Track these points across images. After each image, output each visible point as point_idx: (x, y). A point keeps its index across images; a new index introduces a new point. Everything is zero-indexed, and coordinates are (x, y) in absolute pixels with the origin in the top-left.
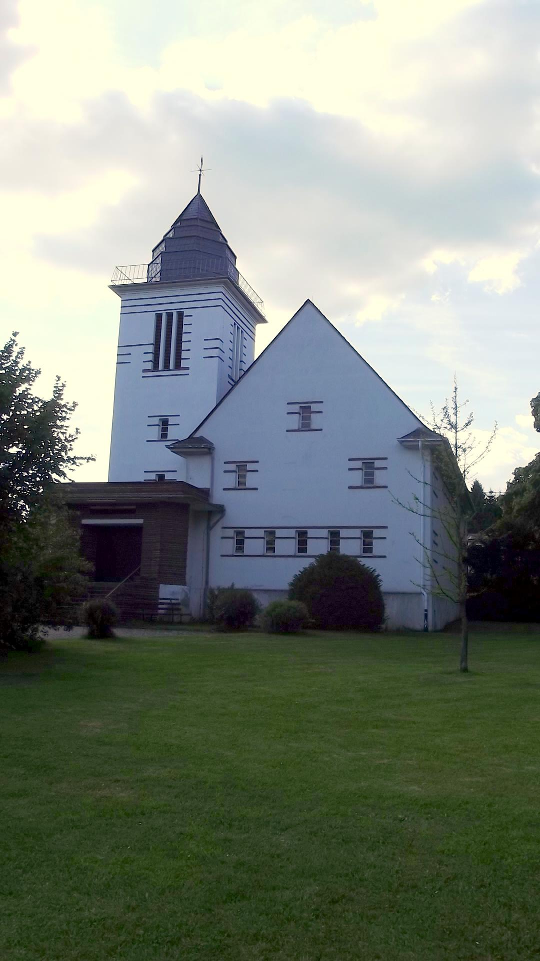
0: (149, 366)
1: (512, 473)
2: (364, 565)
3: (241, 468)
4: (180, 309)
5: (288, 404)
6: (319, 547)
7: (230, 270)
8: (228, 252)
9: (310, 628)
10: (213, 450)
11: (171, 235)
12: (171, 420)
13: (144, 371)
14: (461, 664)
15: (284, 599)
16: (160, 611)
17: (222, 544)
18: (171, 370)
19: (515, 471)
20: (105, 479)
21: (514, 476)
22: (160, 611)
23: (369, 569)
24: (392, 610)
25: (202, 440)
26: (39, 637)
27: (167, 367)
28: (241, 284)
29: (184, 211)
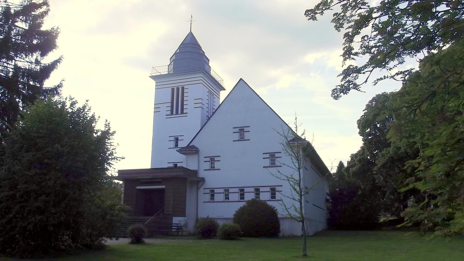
0: (169, 113)
1: (350, 157)
2: (269, 205)
3: (212, 160)
4: (173, 87)
5: (233, 128)
6: (249, 197)
7: (206, 67)
8: (205, 58)
9: (241, 236)
10: (199, 151)
11: (178, 51)
12: (180, 138)
13: (167, 115)
14: (303, 252)
15: (231, 223)
16: (173, 230)
17: (204, 197)
18: (179, 114)
19: (351, 156)
20: (150, 168)
21: (351, 158)
22: (173, 230)
23: (272, 206)
24: (285, 227)
25: (193, 147)
26: (103, 243)
27: (177, 113)
28: (212, 73)
29: (184, 40)
